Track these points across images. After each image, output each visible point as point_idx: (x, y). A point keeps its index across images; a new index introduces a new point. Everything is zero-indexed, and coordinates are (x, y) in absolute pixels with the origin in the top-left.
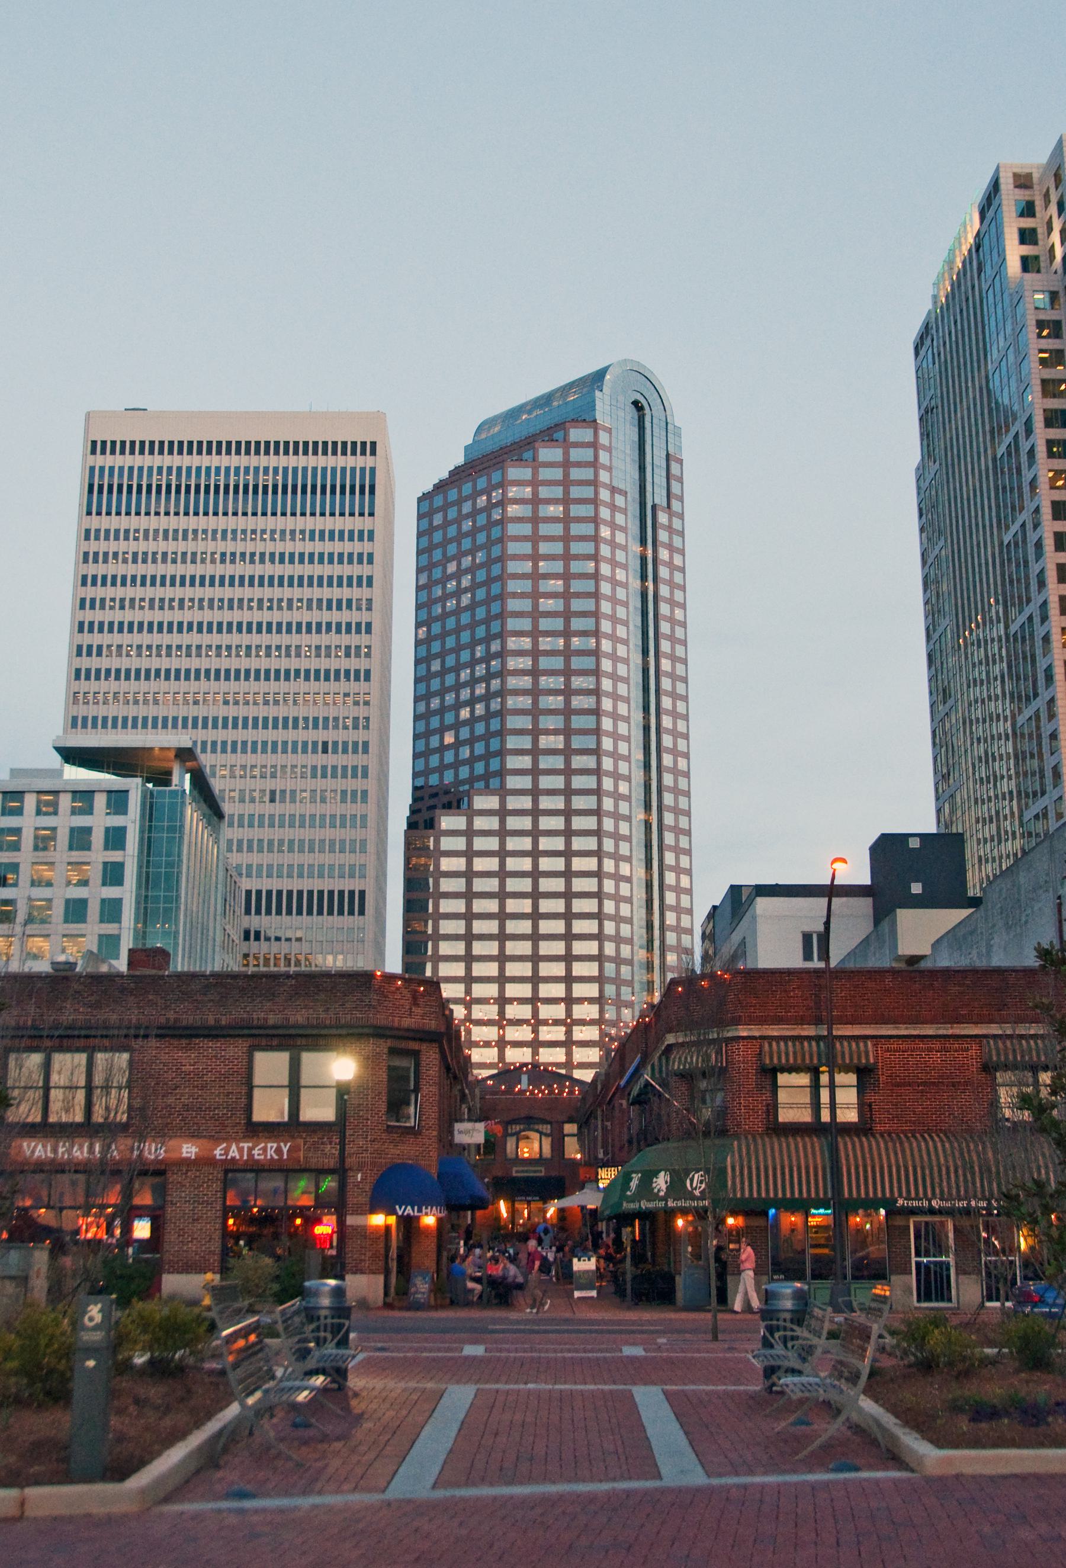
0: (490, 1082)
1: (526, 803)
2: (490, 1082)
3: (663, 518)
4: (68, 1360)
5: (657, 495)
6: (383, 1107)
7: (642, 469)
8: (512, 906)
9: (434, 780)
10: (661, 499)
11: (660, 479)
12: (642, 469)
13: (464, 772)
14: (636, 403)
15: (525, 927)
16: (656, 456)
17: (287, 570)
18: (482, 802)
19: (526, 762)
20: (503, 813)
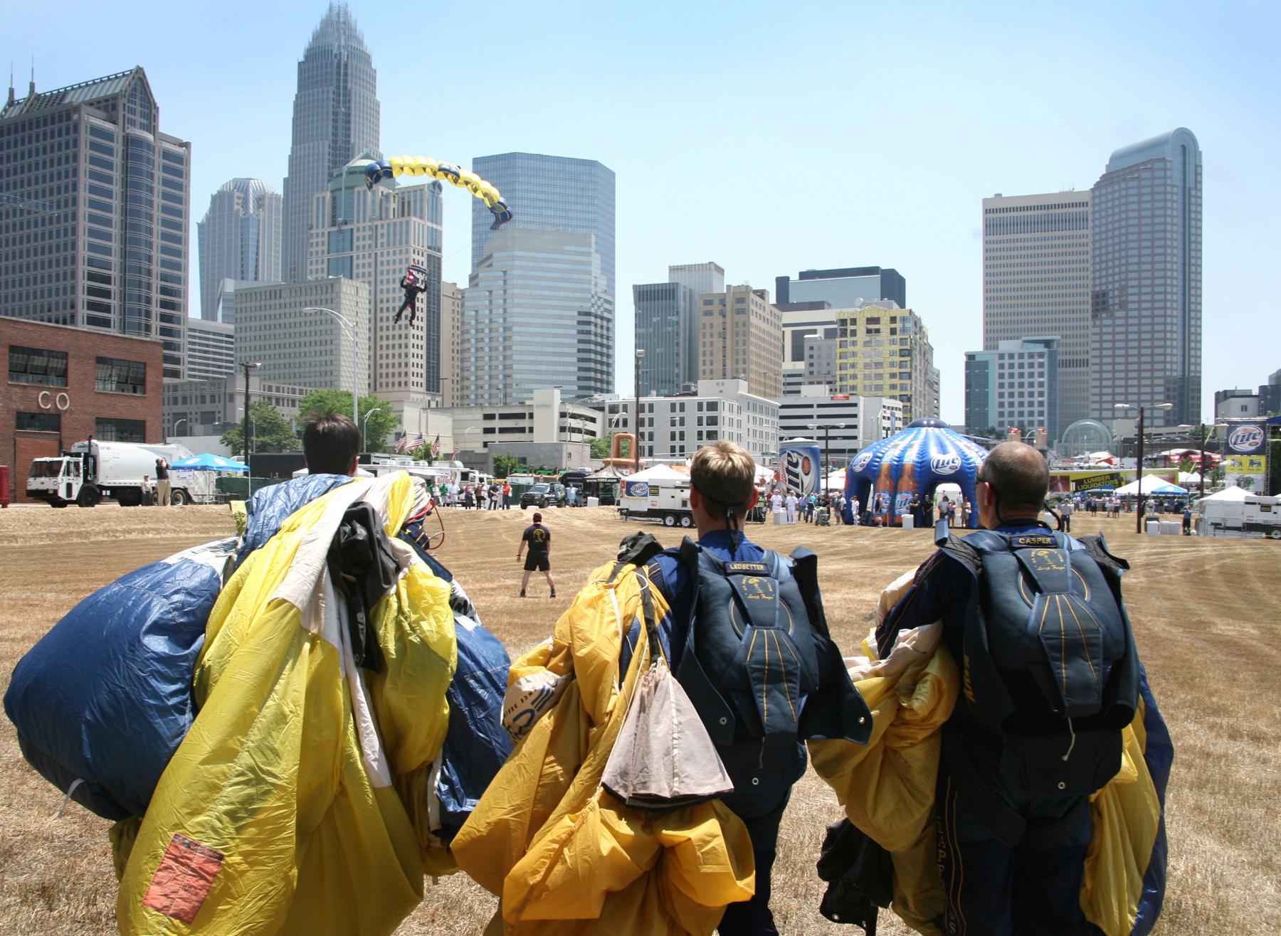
0: (836, 917)
1: (1136, 313)
2: (836, 917)
3: (1193, 193)
4: (1146, 498)
5: (1190, 184)
6: (13, 422)
7: (1184, 173)
8: (1131, 352)
9: (1097, 289)
10: (1192, 185)
11: (1192, 176)
12: (1184, 173)
13: (1110, 287)
14: (1184, 147)
15: (1144, 328)
16: (1190, 168)
17: (1072, 283)
18: (1118, 314)
19: (1136, 298)
20: (1127, 318)
